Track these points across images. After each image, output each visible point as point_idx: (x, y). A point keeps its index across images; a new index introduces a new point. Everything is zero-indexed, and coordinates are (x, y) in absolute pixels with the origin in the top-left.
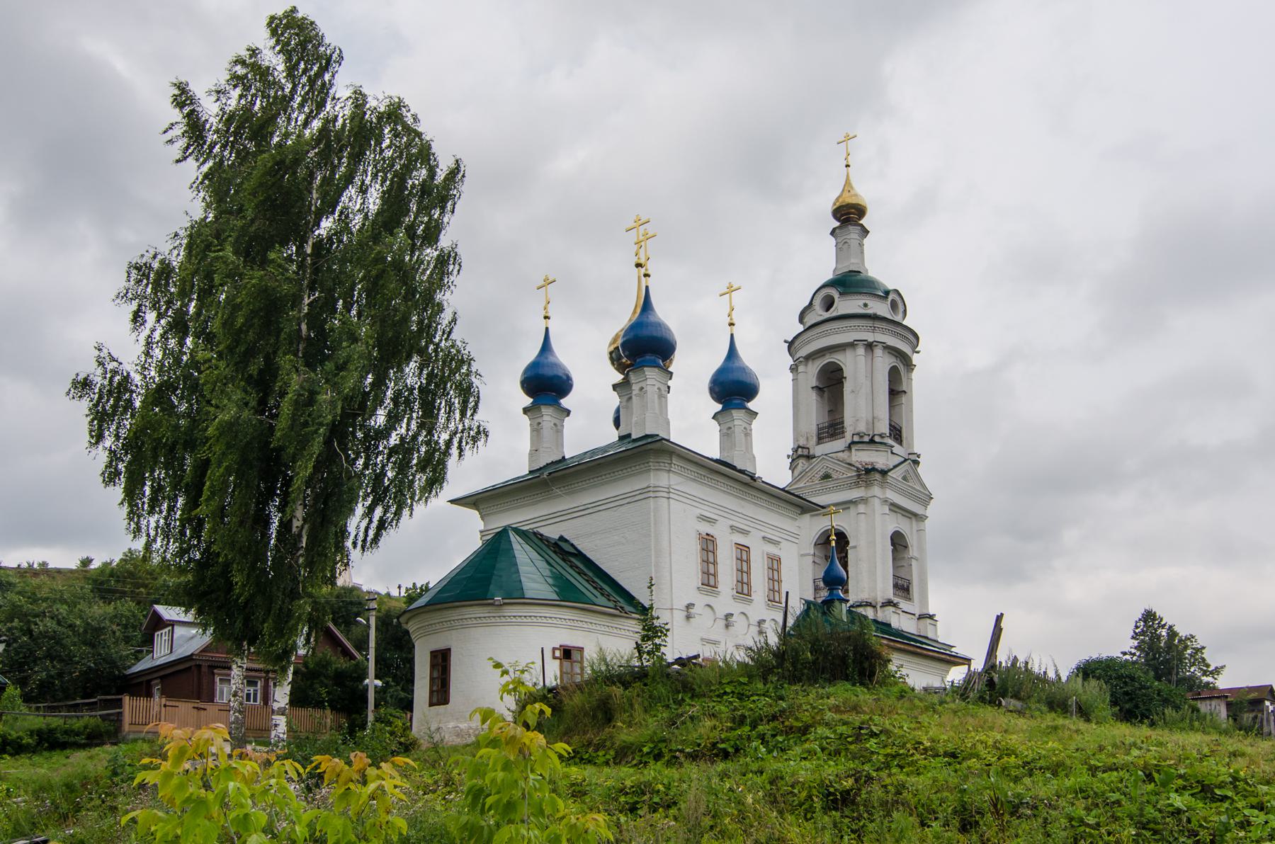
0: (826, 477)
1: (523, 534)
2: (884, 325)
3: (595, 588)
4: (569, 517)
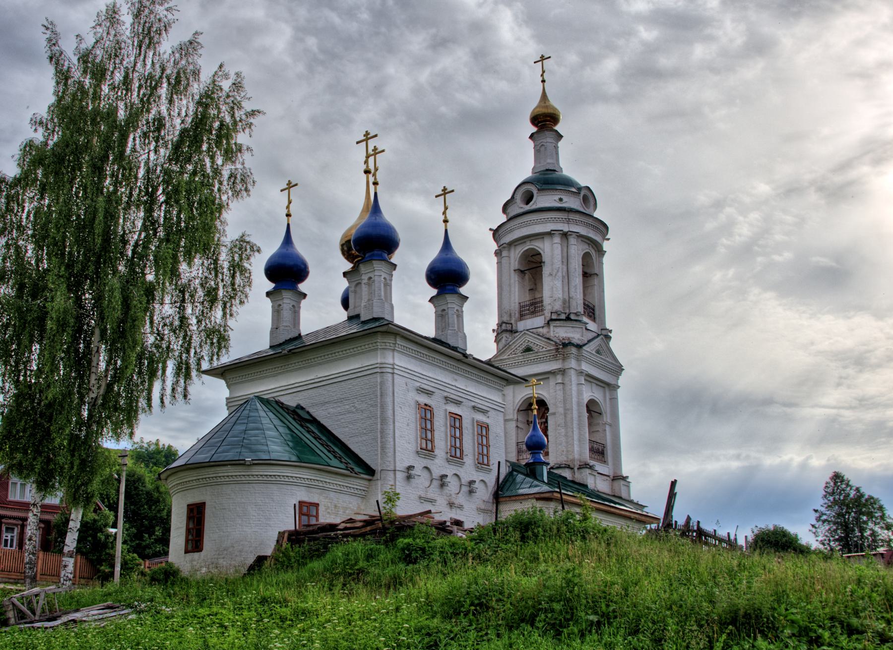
0: (528, 350)
1: (265, 402)
2: (577, 217)
3: (329, 451)
4: (305, 388)
